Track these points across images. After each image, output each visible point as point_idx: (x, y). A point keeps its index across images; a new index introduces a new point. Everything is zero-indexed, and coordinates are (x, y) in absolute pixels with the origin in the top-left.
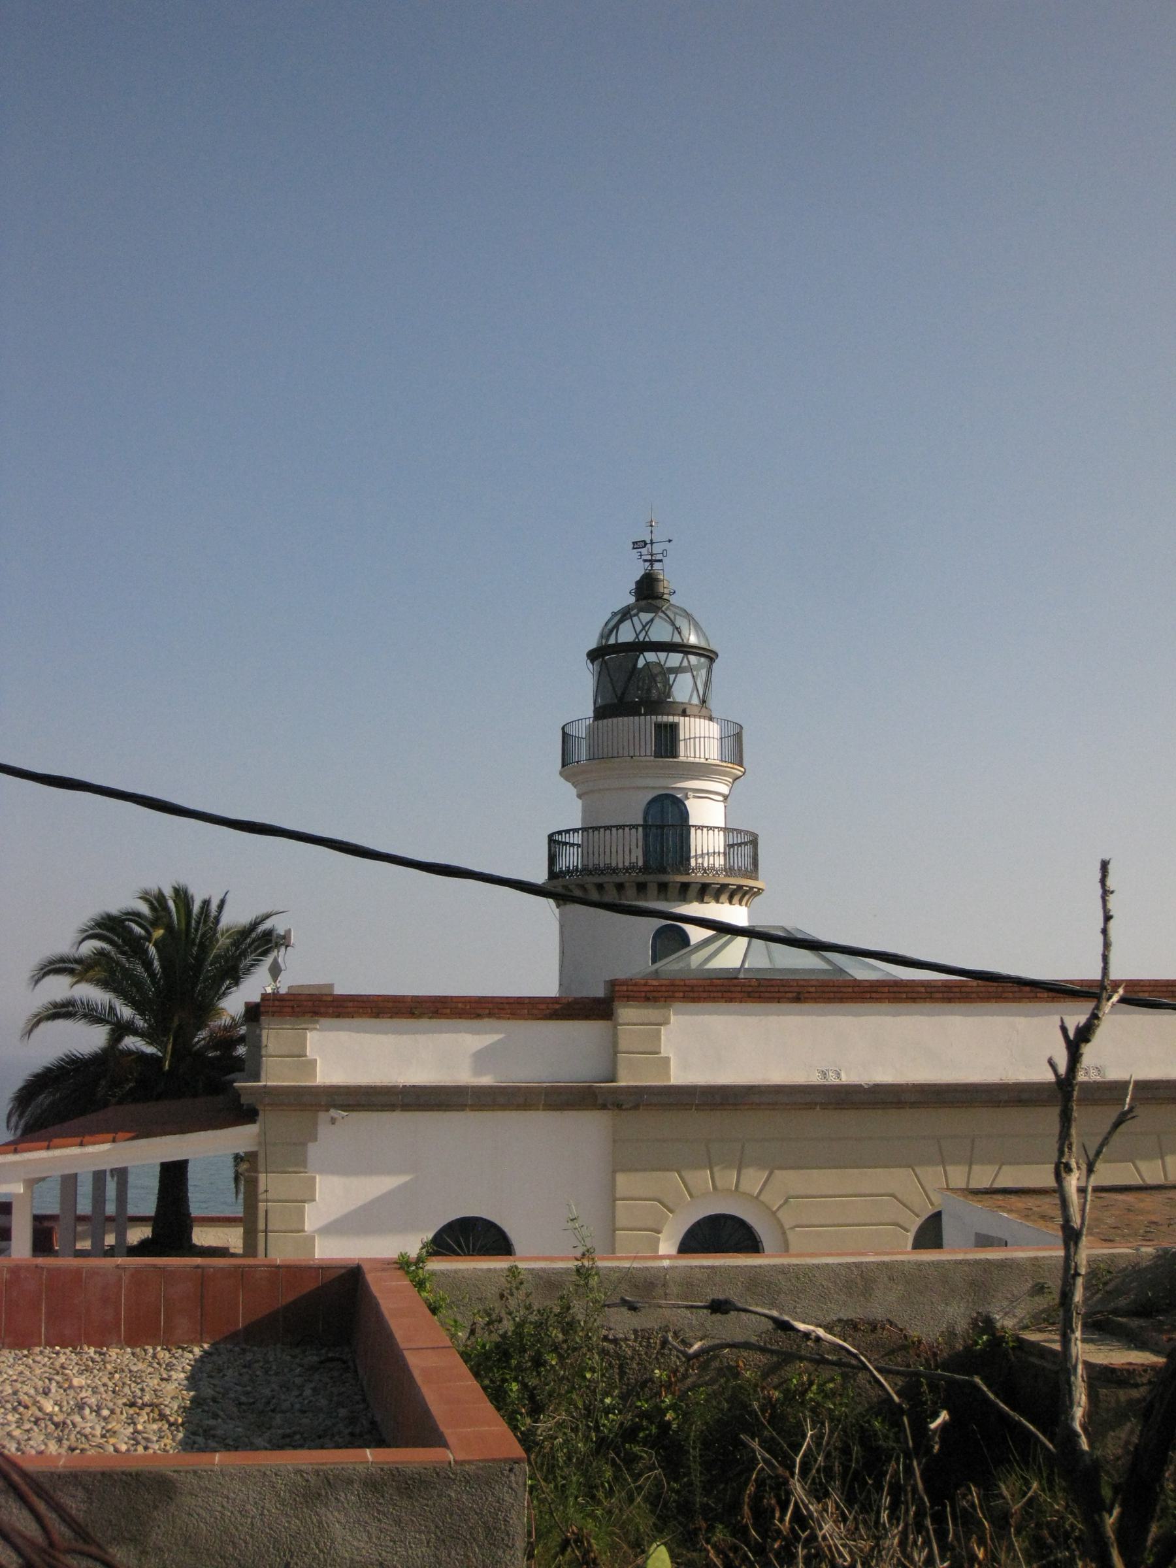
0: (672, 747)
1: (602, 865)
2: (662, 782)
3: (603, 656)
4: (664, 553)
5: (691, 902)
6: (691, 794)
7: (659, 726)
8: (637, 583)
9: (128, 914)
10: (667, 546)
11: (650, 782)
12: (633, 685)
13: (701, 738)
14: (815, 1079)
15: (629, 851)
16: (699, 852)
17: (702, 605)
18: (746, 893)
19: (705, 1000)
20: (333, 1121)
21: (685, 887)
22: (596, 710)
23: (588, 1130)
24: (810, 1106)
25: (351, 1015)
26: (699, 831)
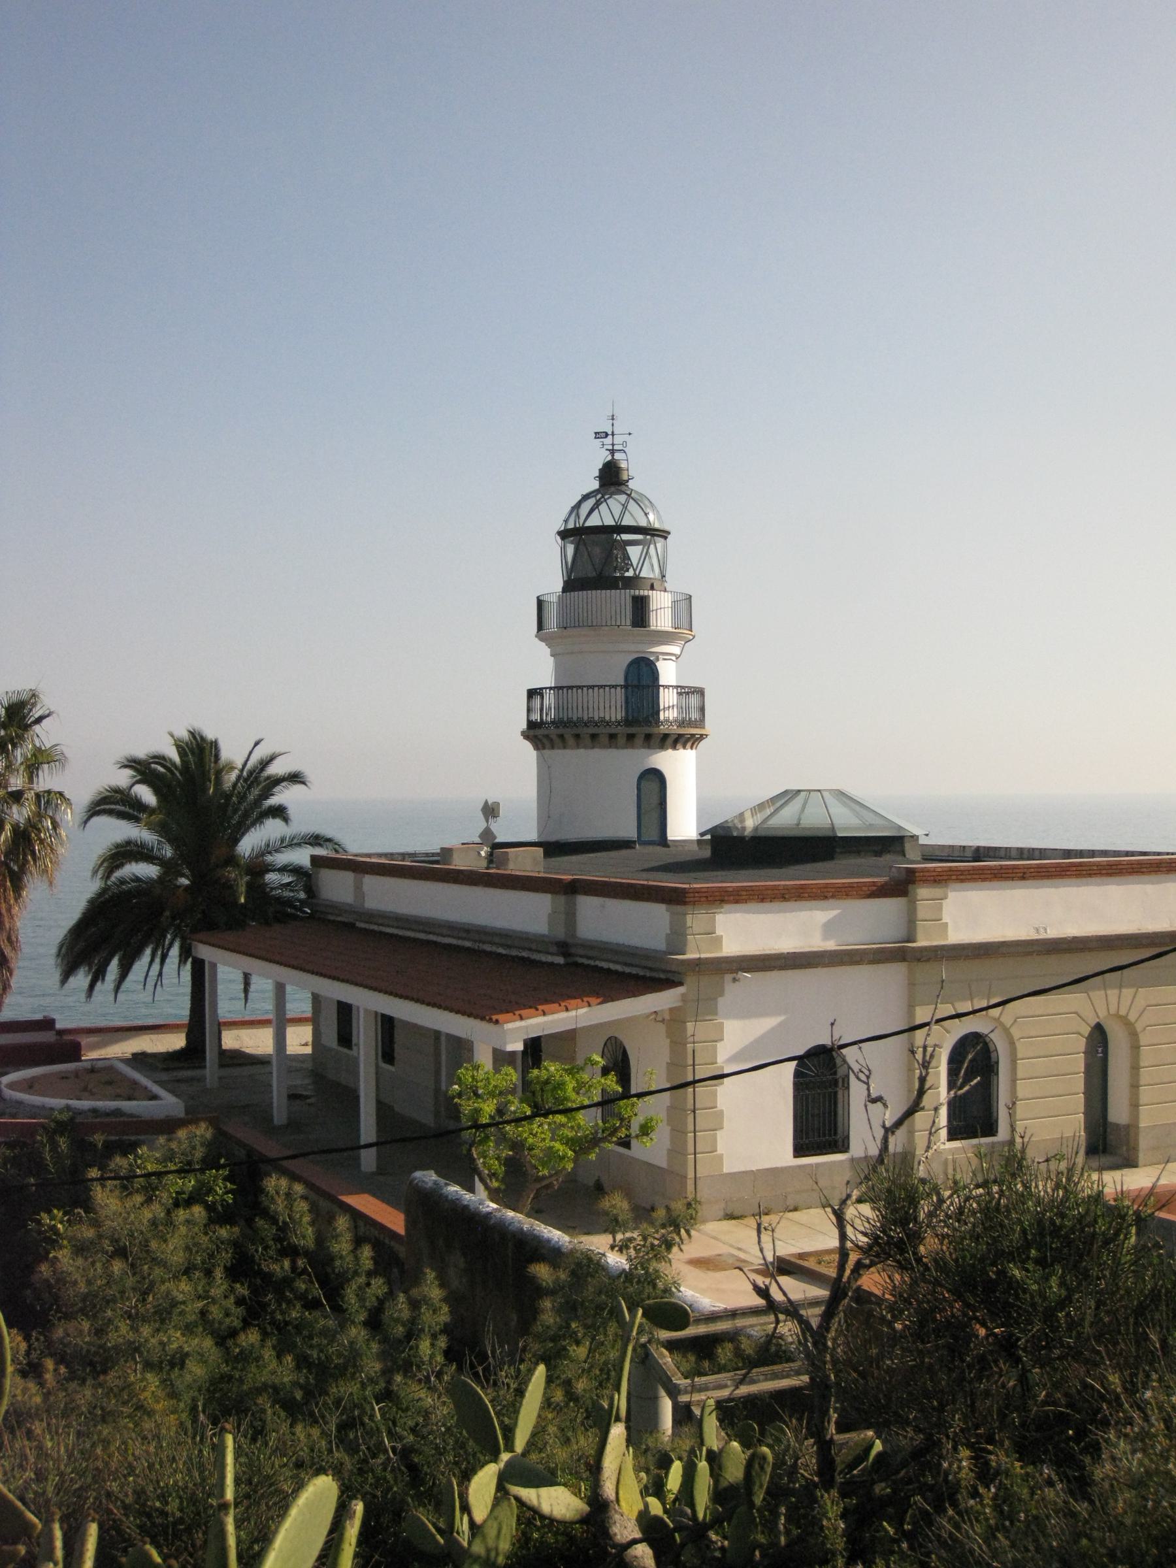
1: (586, 718)
2: (640, 647)
4: (625, 443)
6: (661, 657)
9: (155, 757)
10: (626, 438)
11: (632, 647)
12: (601, 563)
13: (662, 617)
14: (1034, 936)
15: (612, 708)
17: (657, 492)
18: (688, 740)
19: (969, 880)
20: (735, 980)
21: (666, 736)
22: (566, 583)
23: (895, 973)
24: (1030, 954)
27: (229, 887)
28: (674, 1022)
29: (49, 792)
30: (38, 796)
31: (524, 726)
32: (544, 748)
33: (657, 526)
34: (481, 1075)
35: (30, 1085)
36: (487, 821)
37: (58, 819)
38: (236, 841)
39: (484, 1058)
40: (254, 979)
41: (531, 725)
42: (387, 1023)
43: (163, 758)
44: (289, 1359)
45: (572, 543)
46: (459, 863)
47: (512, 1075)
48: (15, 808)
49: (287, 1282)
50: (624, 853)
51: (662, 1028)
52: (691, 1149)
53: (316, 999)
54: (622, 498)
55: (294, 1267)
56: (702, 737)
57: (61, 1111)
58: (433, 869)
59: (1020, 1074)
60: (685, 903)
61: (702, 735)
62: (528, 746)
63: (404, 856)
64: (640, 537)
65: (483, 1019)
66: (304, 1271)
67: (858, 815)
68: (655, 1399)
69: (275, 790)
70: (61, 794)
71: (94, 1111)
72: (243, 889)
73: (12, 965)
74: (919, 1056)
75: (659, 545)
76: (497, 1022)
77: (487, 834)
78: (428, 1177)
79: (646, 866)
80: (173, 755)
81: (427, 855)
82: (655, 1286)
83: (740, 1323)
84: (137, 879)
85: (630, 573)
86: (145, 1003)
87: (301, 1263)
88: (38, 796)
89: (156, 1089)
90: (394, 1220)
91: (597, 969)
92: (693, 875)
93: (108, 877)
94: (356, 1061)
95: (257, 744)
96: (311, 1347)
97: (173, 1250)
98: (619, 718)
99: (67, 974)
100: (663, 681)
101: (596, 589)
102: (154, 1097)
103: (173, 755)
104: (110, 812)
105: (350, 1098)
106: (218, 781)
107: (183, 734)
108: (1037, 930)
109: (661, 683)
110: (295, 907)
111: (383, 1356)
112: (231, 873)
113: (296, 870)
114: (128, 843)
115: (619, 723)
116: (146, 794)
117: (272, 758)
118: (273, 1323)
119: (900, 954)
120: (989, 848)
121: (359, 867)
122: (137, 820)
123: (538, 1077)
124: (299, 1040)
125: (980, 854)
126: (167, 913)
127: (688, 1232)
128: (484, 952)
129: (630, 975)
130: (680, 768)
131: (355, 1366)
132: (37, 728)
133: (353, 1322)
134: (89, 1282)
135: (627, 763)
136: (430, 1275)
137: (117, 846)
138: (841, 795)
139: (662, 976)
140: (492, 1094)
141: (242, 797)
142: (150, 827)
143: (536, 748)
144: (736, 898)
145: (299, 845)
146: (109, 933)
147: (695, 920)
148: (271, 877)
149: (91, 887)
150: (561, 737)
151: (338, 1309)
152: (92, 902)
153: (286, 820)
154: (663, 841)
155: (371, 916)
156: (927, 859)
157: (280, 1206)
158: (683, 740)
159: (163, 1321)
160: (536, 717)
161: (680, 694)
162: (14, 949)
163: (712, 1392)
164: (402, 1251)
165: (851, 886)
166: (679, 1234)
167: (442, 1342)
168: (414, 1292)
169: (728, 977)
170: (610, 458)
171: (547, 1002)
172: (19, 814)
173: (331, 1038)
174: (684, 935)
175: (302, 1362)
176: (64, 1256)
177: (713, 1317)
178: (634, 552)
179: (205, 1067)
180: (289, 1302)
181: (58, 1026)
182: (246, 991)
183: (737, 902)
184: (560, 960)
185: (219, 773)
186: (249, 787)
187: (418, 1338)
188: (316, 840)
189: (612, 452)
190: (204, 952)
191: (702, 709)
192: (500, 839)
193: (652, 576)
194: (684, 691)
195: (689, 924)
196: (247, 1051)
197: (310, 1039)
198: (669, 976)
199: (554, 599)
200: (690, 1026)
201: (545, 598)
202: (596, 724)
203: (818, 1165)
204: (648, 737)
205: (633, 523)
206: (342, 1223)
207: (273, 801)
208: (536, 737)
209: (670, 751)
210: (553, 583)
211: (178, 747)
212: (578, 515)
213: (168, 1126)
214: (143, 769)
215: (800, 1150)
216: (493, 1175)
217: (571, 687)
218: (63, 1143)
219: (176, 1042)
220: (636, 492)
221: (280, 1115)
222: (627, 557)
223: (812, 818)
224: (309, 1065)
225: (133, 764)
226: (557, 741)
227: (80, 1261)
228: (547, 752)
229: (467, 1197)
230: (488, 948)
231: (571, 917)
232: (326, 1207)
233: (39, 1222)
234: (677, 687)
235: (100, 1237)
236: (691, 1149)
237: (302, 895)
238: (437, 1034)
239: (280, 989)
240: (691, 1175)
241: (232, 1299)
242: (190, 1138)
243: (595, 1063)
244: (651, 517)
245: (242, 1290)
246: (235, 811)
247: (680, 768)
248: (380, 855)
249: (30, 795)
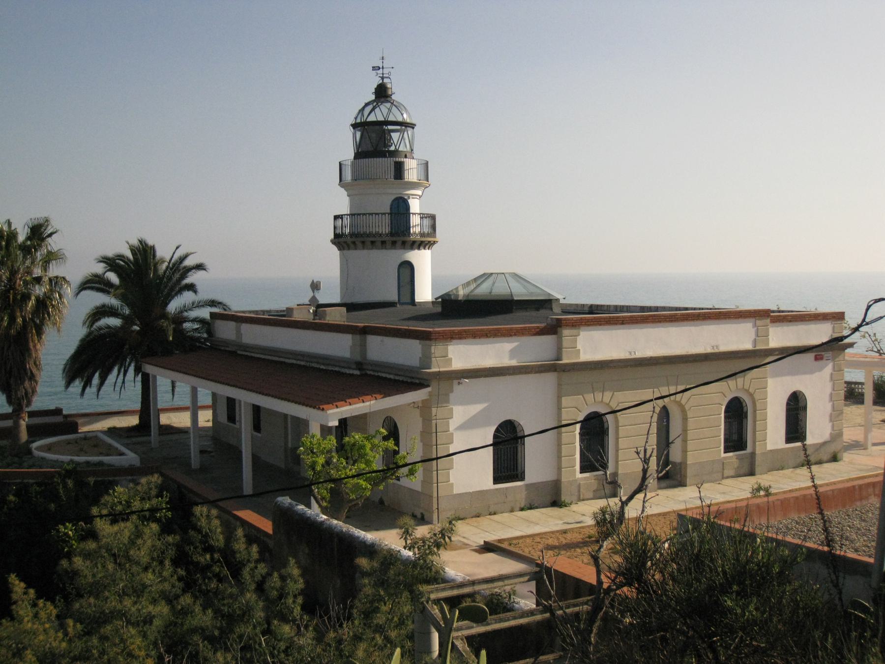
12: (376, 143)
13: (412, 171)
14: (628, 356)
15: (383, 227)
17: (408, 101)
20: (459, 383)
21: (414, 242)
23: (550, 378)
24: (626, 366)
27: (163, 331)
28: (425, 408)
29: (57, 277)
30: (50, 280)
33: (408, 121)
34: (315, 441)
35: (49, 448)
37: (62, 292)
38: (167, 304)
39: (315, 429)
40: (178, 384)
41: (337, 236)
42: (257, 410)
43: (123, 256)
44: (210, 611)
46: (297, 316)
47: (332, 441)
48: (37, 287)
49: (208, 567)
50: (392, 309)
51: (417, 412)
52: (435, 481)
53: (214, 396)
54: (388, 105)
55: (212, 558)
56: (435, 242)
57: (68, 464)
58: (281, 320)
59: (620, 435)
60: (430, 339)
62: (334, 248)
63: (264, 312)
64: (398, 127)
65: (314, 408)
66: (219, 561)
67: (524, 287)
68: (429, 634)
69: (190, 273)
70: (64, 278)
71: (88, 463)
72: (171, 332)
73: (37, 379)
74: (642, 455)
76: (323, 409)
78: (285, 500)
79: (405, 316)
80: (129, 254)
81: (277, 311)
82: (431, 570)
83: (477, 588)
84: (108, 327)
85: (392, 148)
86: (115, 399)
87: (216, 556)
88: (50, 280)
89: (123, 449)
90: (266, 525)
91: (379, 377)
92: (436, 322)
93: (92, 326)
94: (239, 431)
95: (177, 248)
96: (224, 605)
97: (142, 554)
99: (68, 384)
100: (411, 211)
102: (122, 454)
103: (129, 254)
104: (92, 288)
105: (235, 453)
106: (156, 270)
107: (135, 242)
108: (630, 353)
110: (201, 342)
111: (266, 609)
112: (164, 323)
113: (202, 321)
114: (104, 306)
116: (113, 277)
117: (186, 256)
118: (200, 591)
119: (554, 367)
120: (598, 306)
121: (239, 319)
122: (108, 293)
123: (348, 442)
124: (205, 418)
125: (593, 309)
126: (127, 347)
127: (449, 538)
129: (403, 382)
130: (423, 261)
131: (249, 616)
132: (49, 240)
133: (248, 590)
134: (94, 576)
135: (393, 257)
136: (292, 561)
137: (97, 308)
138: (516, 276)
139: (417, 381)
140: (323, 453)
141: (170, 279)
142: (116, 296)
143: (339, 249)
144: (460, 336)
145: (203, 306)
146: (94, 358)
147: (436, 349)
148: (187, 325)
149: (81, 332)
150: (354, 243)
151: (240, 583)
152: (82, 341)
153: (195, 292)
154: (413, 302)
155: (246, 347)
156: (565, 312)
157: (203, 522)
159: (138, 597)
160: (339, 231)
162: (38, 369)
163: (464, 630)
164: (271, 543)
165: (525, 328)
166: (444, 539)
167: (300, 600)
168: (283, 571)
169: (455, 382)
171: (351, 397)
172: (39, 290)
173: (223, 419)
174: (431, 358)
175: (217, 612)
176: (78, 561)
177: (462, 585)
178: (395, 136)
179: (150, 435)
180: (209, 578)
181: (64, 412)
182: (173, 390)
183: (460, 338)
184: (357, 372)
185: (155, 265)
186: (173, 274)
187: (286, 598)
188: (213, 303)
189: (383, 78)
190: (149, 369)
191: (434, 227)
194: (423, 216)
195: (433, 351)
196: (175, 425)
197: (211, 418)
198: (422, 381)
199: (349, 163)
200: (434, 410)
203: (507, 488)
206: (240, 532)
207: (188, 281)
208: (339, 243)
209: (416, 251)
210: (348, 153)
211: (132, 250)
213: (132, 472)
214: (111, 263)
215: (496, 480)
216: (323, 498)
217: (359, 214)
218: (70, 483)
219: (134, 421)
221: (195, 461)
223: (500, 289)
224: (211, 433)
225: (106, 260)
226: (352, 246)
227: (88, 563)
228: (345, 252)
229: (309, 512)
230: (314, 365)
231: (363, 346)
232: (230, 524)
233: (58, 531)
235: (100, 548)
236: (435, 481)
237: (205, 335)
238: (286, 416)
239: (194, 392)
240: (435, 495)
241: (175, 577)
242: (149, 483)
243: (381, 433)
244: (405, 116)
245: (181, 572)
246: (166, 287)
247: (423, 261)
248: (250, 312)
249: (46, 279)
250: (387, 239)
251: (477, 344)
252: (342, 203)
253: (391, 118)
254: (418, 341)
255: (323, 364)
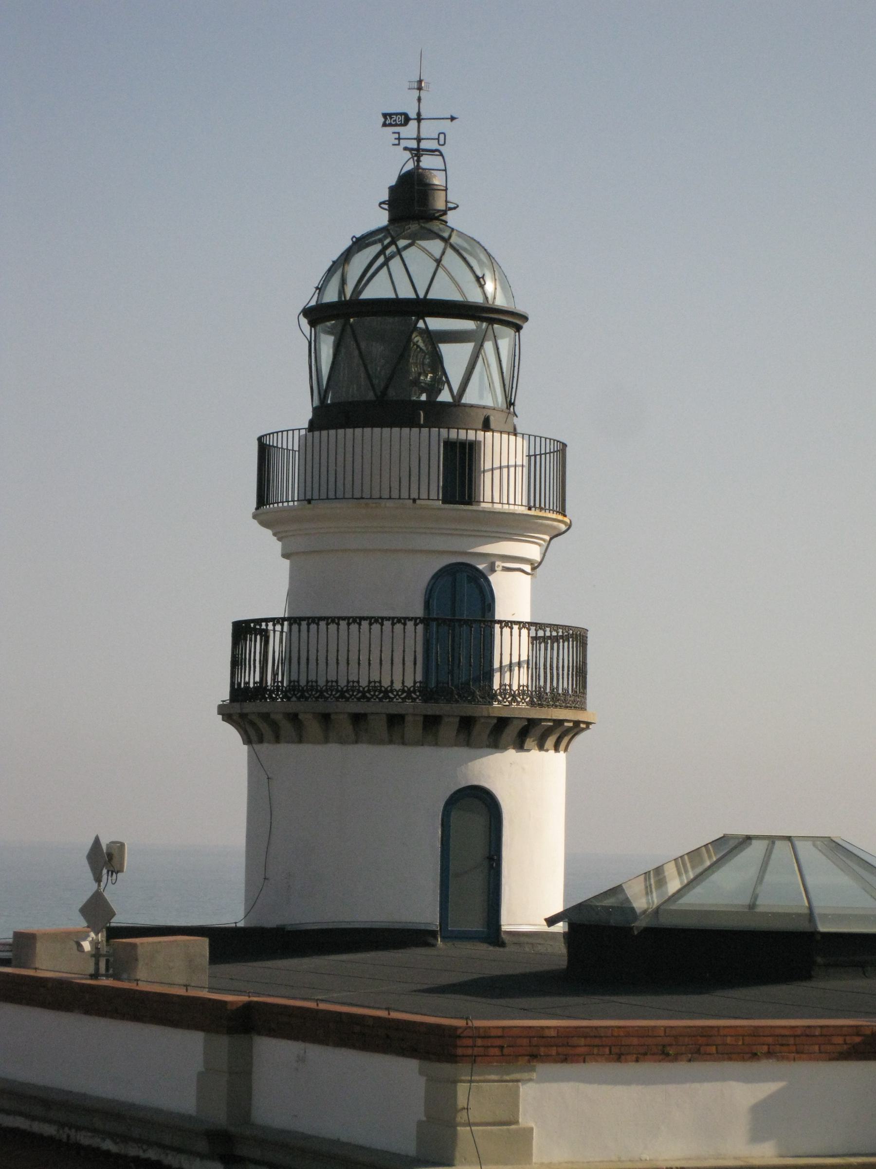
0: (470, 488)
2: (456, 544)
3: (347, 316)
5: (505, 748)
6: (499, 564)
7: (450, 446)
8: (392, 189)
11: (439, 543)
12: (388, 372)
13: (505, 471)
15: (398, 663)
16: (506, 662)
17: (507, 231)
21: (502, 723)
25: (583, 1059)
26: (506, 631)
31: (224, 694)
32: (261, 740)
33: (500, 302)
36: (98, 880)
41: (239, 693)
45: (330, 333)
46: (47, 965)
54: (435, 246)
56: (578, 727)
60: (453, 1058)
61: (577, 723)
62: (231, 735)
64: (468, 325)
75: (505, 345)
77: (96, 910)
79: (419, 987)
85: (445, 396)
98: (409, 683)
100: (501, 613)
101: (391, 425)
108: (302, 1059)
109: (498, 617)
115: (408, 693)
128: (79, 1147)
135: (432, 771)
138: (836, 849)
143: (248, 740)
147: (476, 1094)
150: (294, 718)
154: (492, 931)
158: (537, 731)
160: (252, 678)
161: (534, 639)
165: (807, 1033)
170: (410, 166)
174: (452, 1125)
178: (454, 357)
183: (565, 1059)
189: (417, 153)
191: (581, 672)
192: (120, 920)
193: (488, 401)
195: (461, 1101)
199: (293, 443)
201: (267, 441)
202: (363, 696)
204: (467, 724)
205: (457, 297)
208: (243, 716)
209: (511, 754)
210: (290, 408)
212: (343, 282)
220: (461, 234)
222: (437, 362)
223: (780, 895)
226: (287, 727)
228: (265, 748)
230: (85, 1139)
231: (241, 1077)
234: (531, 624)
244: (489, 286)
247: (534, 789)
250: (407, 707)
251: (628, 1082)
252: (263, 580)
253: (442, 291)
254: (412, 1065)
255: (113, 1136)
